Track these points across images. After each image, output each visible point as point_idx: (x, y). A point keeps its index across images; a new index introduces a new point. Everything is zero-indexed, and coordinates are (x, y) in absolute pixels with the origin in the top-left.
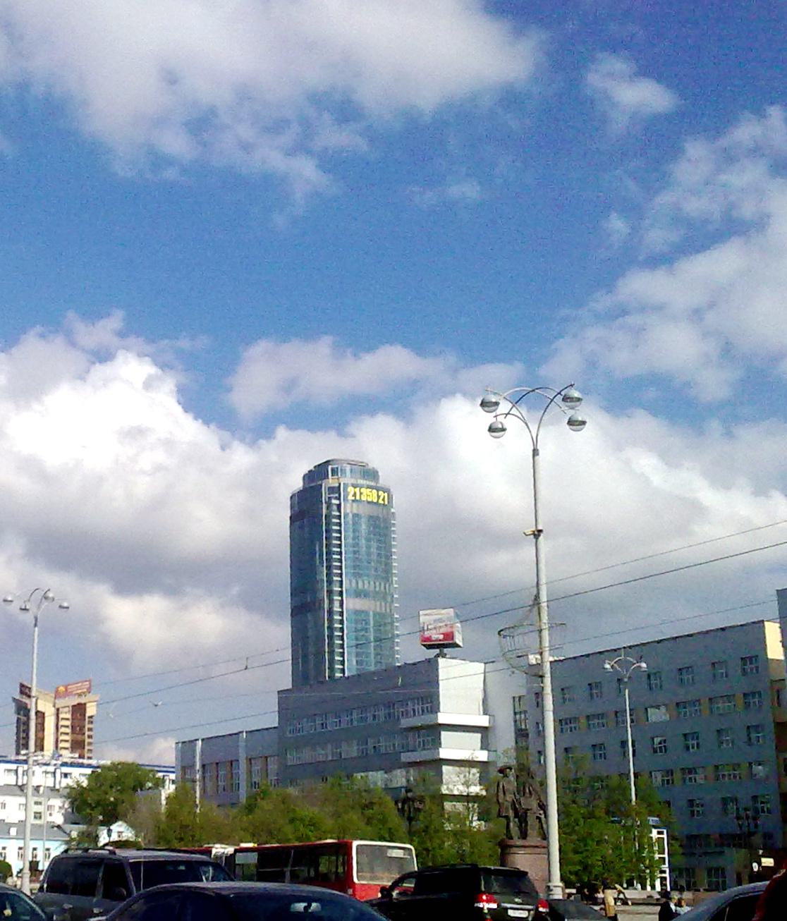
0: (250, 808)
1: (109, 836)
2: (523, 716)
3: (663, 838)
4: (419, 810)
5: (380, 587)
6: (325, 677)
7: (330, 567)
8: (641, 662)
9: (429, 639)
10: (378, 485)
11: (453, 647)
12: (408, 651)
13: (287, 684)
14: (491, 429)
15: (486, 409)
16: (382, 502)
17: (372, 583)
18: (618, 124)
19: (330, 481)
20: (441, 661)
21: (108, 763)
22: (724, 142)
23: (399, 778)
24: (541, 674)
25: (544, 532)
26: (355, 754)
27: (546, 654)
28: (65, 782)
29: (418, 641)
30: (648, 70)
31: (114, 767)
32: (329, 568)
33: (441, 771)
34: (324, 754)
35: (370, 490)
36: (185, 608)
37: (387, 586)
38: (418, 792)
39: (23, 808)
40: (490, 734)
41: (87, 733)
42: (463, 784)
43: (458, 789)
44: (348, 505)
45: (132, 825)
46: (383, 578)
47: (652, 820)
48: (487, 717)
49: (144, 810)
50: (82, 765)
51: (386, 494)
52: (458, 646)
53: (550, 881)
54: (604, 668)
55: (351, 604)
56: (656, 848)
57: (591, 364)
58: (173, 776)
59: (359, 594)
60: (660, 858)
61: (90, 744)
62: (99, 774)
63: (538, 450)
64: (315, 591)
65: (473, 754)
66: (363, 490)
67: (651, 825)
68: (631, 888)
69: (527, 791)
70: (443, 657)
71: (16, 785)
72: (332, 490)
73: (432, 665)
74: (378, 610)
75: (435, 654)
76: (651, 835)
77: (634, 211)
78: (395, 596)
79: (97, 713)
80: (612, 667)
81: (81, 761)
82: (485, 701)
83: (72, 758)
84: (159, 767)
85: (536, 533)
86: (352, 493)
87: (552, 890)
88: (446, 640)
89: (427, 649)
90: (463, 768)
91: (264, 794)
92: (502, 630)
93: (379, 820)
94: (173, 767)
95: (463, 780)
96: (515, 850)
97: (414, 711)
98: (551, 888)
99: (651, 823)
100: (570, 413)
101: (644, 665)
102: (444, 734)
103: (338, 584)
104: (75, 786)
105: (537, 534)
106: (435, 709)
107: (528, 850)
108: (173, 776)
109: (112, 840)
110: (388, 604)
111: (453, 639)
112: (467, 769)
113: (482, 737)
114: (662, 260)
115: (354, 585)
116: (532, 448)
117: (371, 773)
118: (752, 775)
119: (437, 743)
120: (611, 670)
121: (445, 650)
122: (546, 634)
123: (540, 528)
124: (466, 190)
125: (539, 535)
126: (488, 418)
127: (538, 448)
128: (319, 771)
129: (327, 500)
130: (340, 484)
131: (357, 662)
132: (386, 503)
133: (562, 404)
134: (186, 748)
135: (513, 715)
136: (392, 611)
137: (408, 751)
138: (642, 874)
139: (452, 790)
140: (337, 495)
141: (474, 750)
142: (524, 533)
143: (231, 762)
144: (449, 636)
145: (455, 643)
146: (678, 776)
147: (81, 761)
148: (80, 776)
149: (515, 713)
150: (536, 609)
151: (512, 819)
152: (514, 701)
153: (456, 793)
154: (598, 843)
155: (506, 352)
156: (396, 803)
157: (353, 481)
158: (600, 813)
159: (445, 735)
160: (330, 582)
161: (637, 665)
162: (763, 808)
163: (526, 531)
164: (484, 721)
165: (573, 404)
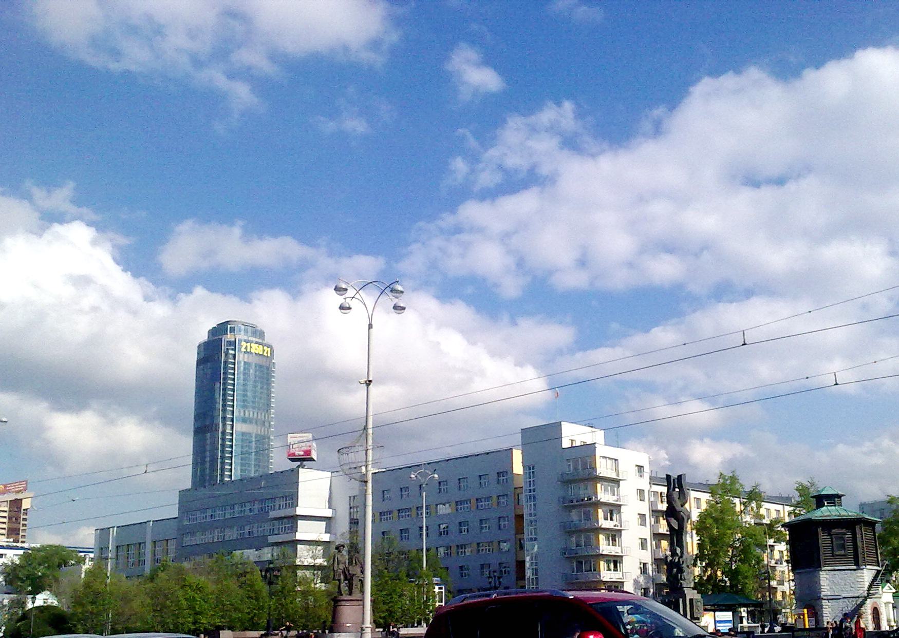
0: (152, 579)
1: (33, 603)
2: (355, 510)
3: (442, 592)
4: (277, 577)
5: (261, 417)
6: (217, 480)
7: (225, 399)
8: (434, 473)
9: (294, 454)
10: (264, 342)
11: (311, 461)
12: (278, 462)
13: (188, 485)
14: (342, 308)
15: (338, 292)
16: (266, 355)
17: (255, 413)
18: (465, 95)
19: (229, 336)
20: (301, 470)
21: (38, 546)
22: (533, 119)
23: (267, 554)
24: (365, 480)
25: (373, 382)
26: (235, 537)
27: (370, 467)
29: (286, 455)
30: (489, 60)
31: (43, 549)
32: (224, 400)
33: (297, 549)
34: (214, 536)
35: (258, 345)
36: (112, 422)
37: (267, 415)
38: (278, 564)
40: (333, 521)
41: (22, 522)
42: (311, 558)
43: (308, 561)
44: (241, 356)
45: (57, 595)
46: (264, 410)
47: (436, 580)
48: (331, 510)
49: (64, 580)
50: (17, 548)
51: (269, 349)
52: (314, 460)
53: (363, 624)
54: (411, 478)
55: (239, 427)
56: (437, 599)
57: (433, 265)
58: (92, 555)
59: (244, 420)
60: (439, 605)
61: (24, 530)
63: (372, 325)
64: (212, 417)
65: (319, 536)
66: (252, 345)
67: (434, 584)
68: (419, 626)
69: (354, 562)
70: (302, 468)
72: (230, 343)
73: (294, 473)
74: (259, 433)
75: (297, 465)
76: (434, 590)
77: (473, 159)
78: (272, 423)
79: (32, 507)
80: (416, 476)
81: (15, 544)
83: (7, 542)
84: (84, 548)
85: (367, 382)
86: (244, 347)
87: (364, 630)
88: (305, 455)
89: (292, 461)
90: (311, 547)
91: (165, 568)
92: (340, 449)
93: (249, 585)
94: (93, 549)
95: (311, 554)
96: (343, 603)
97: (280, 505)
98: (363, 629)
99: (435, 582)
100: (396, 301)
101: (436, 476)
102: (300, 522)
103: (230, 413)
104: (10, 564)
105: (368, 383)
106: (295, 504)
107: (355, 603)
108: (92, 555)
109: (35, 605)
110: (266, 429)
111: (310, 455)
112: (315, 547)
114: (490, 195)
115: (242, 414)
116: (369, 323)
117: (246, 550)
118: (500, 550)
119: (294, 529)
120: (415, 479)
121: (305, 463)
122: (370, 452)
123: (370, 379)
124: (356, 126)
125: (370, 384)
126: (339, 300)
127: (372, 323)
128: (207, 549)
129: (226, 350)
130: (235, 339)
131: (241, 469)
132: (269, 355)
133: (390, 294)
134: (103, 533)
135: (348, 509)
136: (269, 434)
137: (274, 535)
138: (427, 617)
139: (303, 562)
140: (233, 347)
141: (320, 533)
142: (360, 382)
143: (140, 544)
144: (308, 453)
145: (312, 458)
146: (454, 550)
147: (15, 544)
149: (351, 508)
150: (364, 436)
151: (342, 581)
152: (350, 500)
153: (306, 564)
154: (400, 597)
156: (261, 571)
157: (246, 338)
158: (403, 575)
159: (300, 523)
160: (224, 410)
161: (432, 476)
162: (505, 571)
163: (360, 381)
164: (328, 513)
165: (397, 294)
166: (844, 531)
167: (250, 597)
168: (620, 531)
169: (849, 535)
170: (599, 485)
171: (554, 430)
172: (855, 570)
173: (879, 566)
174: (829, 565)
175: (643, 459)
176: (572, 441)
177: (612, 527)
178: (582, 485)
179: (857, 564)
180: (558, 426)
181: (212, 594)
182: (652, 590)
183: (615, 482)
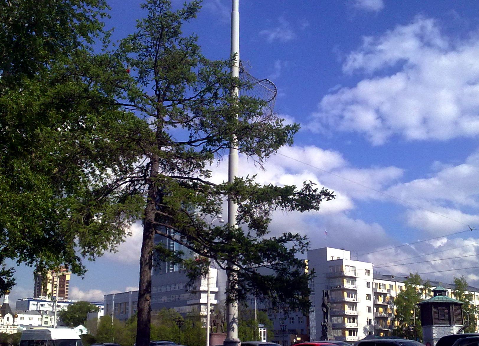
28: (58, 309)
39: (40, 320)
41: (66, 287)
58: (103, 307)
61: (67, 292)
62: (73, 306)
71: (37, 310)
82: (217, 283)
109: (83, 334)
113: (215, 296)
148: (64, 307)
155: (161, 274)
166: (444, 308)
167: (173, 332)
168: (356, 303)
169: (446, 311)
170: (345, 280)
171: (323, 252)
172: (449, 326)
173: (463, 325)
174: (437, 324)
175: (369, 266)
176: (332, 257)
177: (352, 301)
178: (337, 280)
179: (450, 324)
180: (325, 251)
181: (157, 330)
182: (374, 333)
183: (353, 279)
